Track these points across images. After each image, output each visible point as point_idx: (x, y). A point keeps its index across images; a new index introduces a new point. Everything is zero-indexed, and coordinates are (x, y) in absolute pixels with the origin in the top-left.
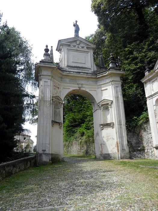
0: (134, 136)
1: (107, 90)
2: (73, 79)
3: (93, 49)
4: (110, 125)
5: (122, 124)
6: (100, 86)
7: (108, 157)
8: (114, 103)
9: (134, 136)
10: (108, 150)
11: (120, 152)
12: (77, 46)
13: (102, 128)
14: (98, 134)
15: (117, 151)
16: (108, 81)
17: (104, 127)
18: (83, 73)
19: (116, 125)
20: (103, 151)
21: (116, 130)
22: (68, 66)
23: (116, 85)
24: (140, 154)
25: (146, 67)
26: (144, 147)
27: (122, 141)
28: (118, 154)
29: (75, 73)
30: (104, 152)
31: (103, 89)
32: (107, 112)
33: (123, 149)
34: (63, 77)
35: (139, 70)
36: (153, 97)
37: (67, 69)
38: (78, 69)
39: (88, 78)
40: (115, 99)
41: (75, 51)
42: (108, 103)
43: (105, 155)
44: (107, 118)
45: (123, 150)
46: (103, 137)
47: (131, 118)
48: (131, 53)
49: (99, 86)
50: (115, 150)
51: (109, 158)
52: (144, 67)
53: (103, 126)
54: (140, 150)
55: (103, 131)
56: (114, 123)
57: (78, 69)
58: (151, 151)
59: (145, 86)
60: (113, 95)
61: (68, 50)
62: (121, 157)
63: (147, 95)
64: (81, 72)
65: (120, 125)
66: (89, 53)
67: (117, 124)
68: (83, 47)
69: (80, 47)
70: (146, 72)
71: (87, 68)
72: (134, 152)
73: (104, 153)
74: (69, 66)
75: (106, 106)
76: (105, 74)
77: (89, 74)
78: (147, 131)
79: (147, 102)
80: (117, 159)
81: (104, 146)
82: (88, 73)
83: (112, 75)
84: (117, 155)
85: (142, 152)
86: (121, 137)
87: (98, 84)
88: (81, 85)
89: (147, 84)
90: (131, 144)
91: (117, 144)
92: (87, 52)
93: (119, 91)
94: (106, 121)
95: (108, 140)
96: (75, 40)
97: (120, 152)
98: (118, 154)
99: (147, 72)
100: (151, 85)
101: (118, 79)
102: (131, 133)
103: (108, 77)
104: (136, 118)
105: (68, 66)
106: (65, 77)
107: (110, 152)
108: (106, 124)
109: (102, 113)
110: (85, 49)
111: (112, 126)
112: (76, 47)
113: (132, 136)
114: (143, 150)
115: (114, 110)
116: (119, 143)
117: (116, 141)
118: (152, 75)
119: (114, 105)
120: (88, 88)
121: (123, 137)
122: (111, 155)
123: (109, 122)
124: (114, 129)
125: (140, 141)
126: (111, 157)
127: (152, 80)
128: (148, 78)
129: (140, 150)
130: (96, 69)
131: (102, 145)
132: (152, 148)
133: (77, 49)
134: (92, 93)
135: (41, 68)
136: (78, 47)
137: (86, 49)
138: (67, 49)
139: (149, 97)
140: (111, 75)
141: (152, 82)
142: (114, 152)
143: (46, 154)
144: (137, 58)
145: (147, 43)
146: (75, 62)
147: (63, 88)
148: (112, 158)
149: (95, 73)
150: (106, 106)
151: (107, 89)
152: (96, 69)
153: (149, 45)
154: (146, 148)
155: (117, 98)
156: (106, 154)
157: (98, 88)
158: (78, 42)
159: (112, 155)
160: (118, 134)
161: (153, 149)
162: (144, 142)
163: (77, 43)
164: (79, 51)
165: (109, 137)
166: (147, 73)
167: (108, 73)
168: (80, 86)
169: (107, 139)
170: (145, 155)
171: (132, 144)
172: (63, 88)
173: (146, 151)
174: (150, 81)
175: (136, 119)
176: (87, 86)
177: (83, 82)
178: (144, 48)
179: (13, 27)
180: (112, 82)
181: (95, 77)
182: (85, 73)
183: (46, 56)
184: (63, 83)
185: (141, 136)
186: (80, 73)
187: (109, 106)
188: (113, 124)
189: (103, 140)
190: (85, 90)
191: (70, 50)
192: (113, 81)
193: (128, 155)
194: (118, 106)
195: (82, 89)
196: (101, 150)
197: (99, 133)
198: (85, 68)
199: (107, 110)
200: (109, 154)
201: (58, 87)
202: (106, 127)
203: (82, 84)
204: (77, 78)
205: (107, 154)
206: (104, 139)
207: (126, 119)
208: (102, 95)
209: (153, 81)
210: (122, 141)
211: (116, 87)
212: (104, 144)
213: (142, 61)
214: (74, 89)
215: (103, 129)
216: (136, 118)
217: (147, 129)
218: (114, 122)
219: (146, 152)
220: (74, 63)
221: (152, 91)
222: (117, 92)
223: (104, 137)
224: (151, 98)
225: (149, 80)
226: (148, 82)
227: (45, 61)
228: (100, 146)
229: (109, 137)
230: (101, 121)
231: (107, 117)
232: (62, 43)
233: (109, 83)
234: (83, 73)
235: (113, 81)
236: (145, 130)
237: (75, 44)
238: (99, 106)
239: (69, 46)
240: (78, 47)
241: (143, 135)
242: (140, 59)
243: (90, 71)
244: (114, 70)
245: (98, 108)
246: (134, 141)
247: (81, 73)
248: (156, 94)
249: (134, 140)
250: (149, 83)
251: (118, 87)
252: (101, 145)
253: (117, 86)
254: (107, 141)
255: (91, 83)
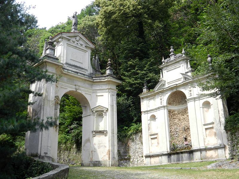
0: (122, 145)
1: (102, 97)
2: (71, 79)
3: (92, 49)
4: (104, 132)
5: (114, 133)
6: (95, 91)
7: (98, 164)
8: (109, 112)
9: (122, 145)
10: (98, 158)
11: (111, 159)
12: (76, 42)
13: (94, 134)
14: (88, 140)
15: (108, 159)
16: (104, 87)
17: (96, 134)
18: (81, 73)
19: (109, 134)
20: (93, 158)
21: (109, 138)
22: (67, 63)
23: (112, 94)
24: (126, 162)
25: (145, 84)
26: (130, 156)
27: (114, 149)
28: (109, 161)
29: (73, 73)
30: (95, 159)
31: (98, 94)
32: (100, 119)
33: (113, 157)
34: (62, 74)
35: (138, 85)
36: (149, 112)
37: (66, 66)
38: (76, 68)
39: (85, 80)
40: (111, 107)
41: (74, 47)
42: (103, 111)
43: (96, 162)
44: (99, 126)
45: (114, 158)
46: (94, 143)
47: (122, 128)
48: (133, 67)
49: (95, 91)
50: (106, 158)
51: (99, 165)
52: (143, 84)
53: (95, 133)
54: (126, 159)
55: (95, 138)
56: (108, 131)
57: (76, 68)
58: (137, 160)
59: (142, 101)
60: (109, 103)
61: (68, 45)
62: (111, 164)
63: (142, 110)
64: (79, 73)
65: (113, 133)
66: (87, 53)
67: (110, 132)
68: (82, 45)
69: (79, 44)
70: (144, 89)
71: (84, 69)
72: (121, 160)
73: (94, 161)
74: (69, 64)
75: (100, 113)
76: (104, 80)
77: (86, 76)
78: (136, 142)
79: (142, 116)
80: (108, 166)
81: (95, 153)
82: (85, 75)
83: (110, 82)
84: (108, 163)
85: (127, 161)
86: (113, 145)
87: (94, 88)
88: (78, 87)
89: (144, 100)
90: (120, 153)
91: (109, 152)
92: (86, 51)
93: (114, 100)
94: (98, 129)
95: (99, 148)
96: (76, 35)
97: (111, 159)
98: (109, 161)
99: (146, 89)
100: (148, 102)
101: (114, 87)
102: (121, 142)
103: (106, 83)
104: (127, 128)
105: (67, 63)
106: (64, 75)
107: (100, 160)
108: (99, 131)
109: (95, 119)
110: (83, 47)
111: (105, 134)
112: (75, 43)
113: (121, 146)
114: (129, 159)
115: (109, 118)
116: (111, 151)
117: (107, 148)
118: (151, 94)
119: (109, 113)
120: (84, 90)
121: (115, 145)
122: (101, 162)
123: (101, 128)
124: (107, 137)
125: (127, 151)
126: (101, 165)
127: (149, 97)
128: (146, 95)
129: (126, 159)
130: (92, 72)
131: (93, 152)
132: (139, 157)
133: (76, 45)
134: (87, 97)
135: (47, 63)
136: (77, 44)
137: (85, 47)
138: (67, 44)
139: (144, 112)
140: (108, 82)
141: (149, 99)
142: (105, 159)
143: (47, 157)
144: (138, 74)
145: (149, 63)
146: (73, 60)
147: (61, 87)
148: (102, 165)
149: (91, 76)
150: (100, 113)
151: (103, 95)
152: (92, 72)
153: (151, 65)
154: (132, 157)
155: (112, 106)
156: (96, 161)
157: (93, 93)
158: (78, 38)
159: (103, 163)
160: (110, 142)
161: (139, 158)
162: (130, 152)
163: (77, 39)
164: (77, 48)
165: (101, 145)
166: (145, 90)
167: (107, 79)
168: (77, 87)
169: (99, 146)
170: (131, 164)
171: (121, 153)
172: (61, 87)
173: (131, 160)
174: (147, 98)
175: (126, 129)
176: (83, 89)
177: (79, 84)
178: (145, 67)
179: (52, 26)
180: (109, 89)
181: (91, 80)
182: (82, 74)
183: (50, 50)
184: (61, 82)
185: (128, 146)
186: (77, 73)
187: (104, 114)
188: (106, 132)
189: (94, 147)
190: (81, 92)
191: (70, 46)
192: (110, 89)
193: (117, 163)
194: (112, 115)
195: (78, 91)
196: (91, 157)
197: (90, 139)
198: (82, 68)
199: (99, 117)
200: (99, 161)
201: (57, 86)
202: (98, 134)
203: (79, 86)
204: (75, 79)
205: (98, 161)
206: (95, 146)
207: (118, 128)
208: (96, 101)
209: (150, 98)
210: (113, 149)
211: (112, 95)
212: (95, 152)
213: (142, 78)
214: (71, 90)
215: (95, 136)
216: (127, 128)
217: (135, 140)
218: (107, 130)
219: (132, 161)
220: (72, 61)
221: (148, 107)
222: (112, 101)
223: (95, 144)
224: (147, 113)
225: (147, 97)
226: (144, 98)
227: (49, 55)
228: (91, 153)
229: (101, 145)
230: (94, 127)
231: (99, 124)
232: (63, 36)
233: (107, 89)
234: (81, 73)
235: (110, 89)
236: (133, 141)
237: (74, 39)
238: (92, 111)
239: (69, 40)
240: (77, 44)
241: (130, 145)
242: (141, 76)
243: (87, 73)
244: (111, 78)
245: (92, 114)
246: (122, 151)
247: (79, 74)
248: (152, 111)
249: (122, 150)
250: (146, 99)
251: (114, 95)
252: (92, 152)
253: (113, 94)
254: (99, 148)
255: (87, 86)
